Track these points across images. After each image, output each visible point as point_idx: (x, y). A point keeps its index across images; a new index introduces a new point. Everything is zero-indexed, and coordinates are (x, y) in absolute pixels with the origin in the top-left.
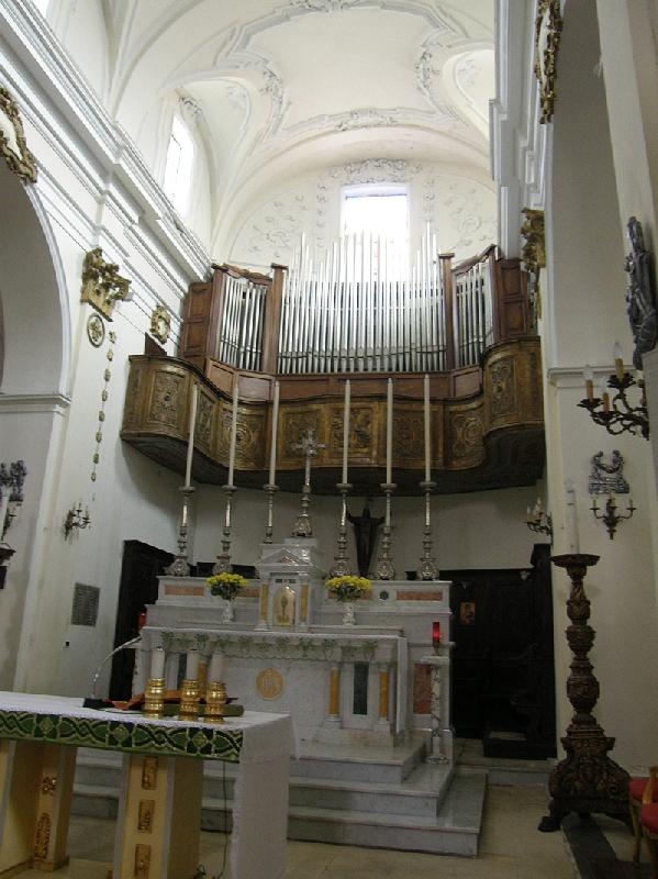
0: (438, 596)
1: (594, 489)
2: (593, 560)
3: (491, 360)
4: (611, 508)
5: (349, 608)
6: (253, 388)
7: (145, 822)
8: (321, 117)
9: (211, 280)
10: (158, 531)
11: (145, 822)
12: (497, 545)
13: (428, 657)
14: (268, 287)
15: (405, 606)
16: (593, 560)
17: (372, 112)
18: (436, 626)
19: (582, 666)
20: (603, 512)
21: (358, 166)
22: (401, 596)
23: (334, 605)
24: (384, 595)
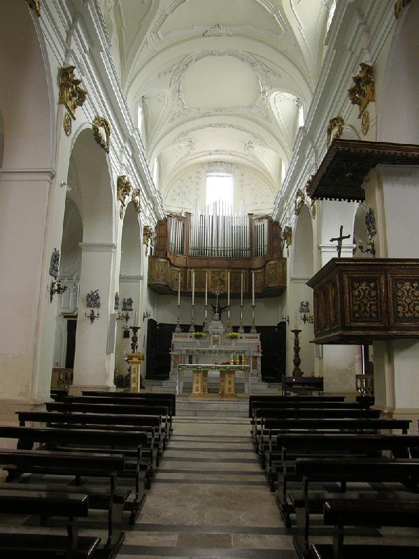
0: (257, 338)
1: (301, 312)
2: (300, 331)
3: (270, 263)
4: (305, 316)
5: (233, 341)
6: (180, 261)
7: (230, 383)
8: (205, 151)
9: (166, 220)
10: (164, 316)
11: (230, 383)
12: (269, 319)
13: (256, 354)
14: (185, 219)
15: (247, 341)
16: (300, 331)
17: (223, 151)
18: (258, 346)
19: (297, 355)
20: (303, 317)
21: (213, 165)
22: (246, 338)
23: (228, 341)
24: (241, 338)
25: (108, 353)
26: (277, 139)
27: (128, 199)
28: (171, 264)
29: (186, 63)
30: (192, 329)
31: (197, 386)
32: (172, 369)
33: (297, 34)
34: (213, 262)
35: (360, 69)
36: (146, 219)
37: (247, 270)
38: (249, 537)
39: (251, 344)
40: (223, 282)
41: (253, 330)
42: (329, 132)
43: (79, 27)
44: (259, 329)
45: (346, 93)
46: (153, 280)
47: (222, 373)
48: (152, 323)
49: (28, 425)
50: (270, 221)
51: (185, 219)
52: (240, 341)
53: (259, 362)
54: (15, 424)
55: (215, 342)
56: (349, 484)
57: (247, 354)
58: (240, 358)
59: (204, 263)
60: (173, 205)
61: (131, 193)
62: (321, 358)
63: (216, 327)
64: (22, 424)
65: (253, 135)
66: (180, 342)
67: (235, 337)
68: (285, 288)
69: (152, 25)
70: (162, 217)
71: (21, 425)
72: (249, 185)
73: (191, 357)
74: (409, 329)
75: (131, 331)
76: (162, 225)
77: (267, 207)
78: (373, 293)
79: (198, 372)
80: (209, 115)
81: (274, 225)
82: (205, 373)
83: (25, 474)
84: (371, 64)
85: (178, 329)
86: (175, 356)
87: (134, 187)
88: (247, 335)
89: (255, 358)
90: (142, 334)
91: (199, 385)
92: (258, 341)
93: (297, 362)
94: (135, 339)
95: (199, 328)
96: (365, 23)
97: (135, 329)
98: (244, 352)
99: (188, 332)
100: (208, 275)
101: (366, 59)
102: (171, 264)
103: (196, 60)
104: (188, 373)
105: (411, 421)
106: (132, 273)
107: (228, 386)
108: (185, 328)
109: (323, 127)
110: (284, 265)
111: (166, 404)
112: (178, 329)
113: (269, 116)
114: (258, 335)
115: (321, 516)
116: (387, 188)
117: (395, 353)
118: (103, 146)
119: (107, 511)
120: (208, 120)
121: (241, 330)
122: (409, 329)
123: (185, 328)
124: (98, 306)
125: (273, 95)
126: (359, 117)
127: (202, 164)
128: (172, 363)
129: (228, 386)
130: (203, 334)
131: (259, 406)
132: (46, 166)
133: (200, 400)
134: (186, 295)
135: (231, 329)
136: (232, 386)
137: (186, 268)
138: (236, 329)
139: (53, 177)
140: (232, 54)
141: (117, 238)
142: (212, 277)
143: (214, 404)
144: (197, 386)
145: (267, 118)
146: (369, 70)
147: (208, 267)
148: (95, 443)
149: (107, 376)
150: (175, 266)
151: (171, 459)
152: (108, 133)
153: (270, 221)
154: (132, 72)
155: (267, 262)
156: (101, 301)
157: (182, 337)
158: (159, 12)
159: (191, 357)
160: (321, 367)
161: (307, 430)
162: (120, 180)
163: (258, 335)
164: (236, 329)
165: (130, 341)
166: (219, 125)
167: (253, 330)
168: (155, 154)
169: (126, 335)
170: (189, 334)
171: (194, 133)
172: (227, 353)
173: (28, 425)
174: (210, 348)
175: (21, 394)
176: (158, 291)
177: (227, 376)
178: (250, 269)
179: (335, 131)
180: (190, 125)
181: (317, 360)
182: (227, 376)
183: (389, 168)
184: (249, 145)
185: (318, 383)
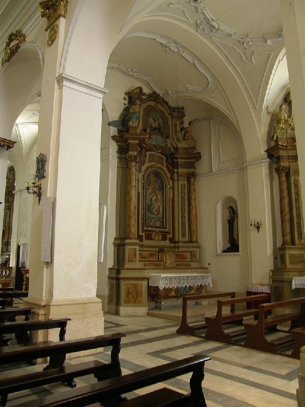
105: (70, 319)
126: (46, 30)
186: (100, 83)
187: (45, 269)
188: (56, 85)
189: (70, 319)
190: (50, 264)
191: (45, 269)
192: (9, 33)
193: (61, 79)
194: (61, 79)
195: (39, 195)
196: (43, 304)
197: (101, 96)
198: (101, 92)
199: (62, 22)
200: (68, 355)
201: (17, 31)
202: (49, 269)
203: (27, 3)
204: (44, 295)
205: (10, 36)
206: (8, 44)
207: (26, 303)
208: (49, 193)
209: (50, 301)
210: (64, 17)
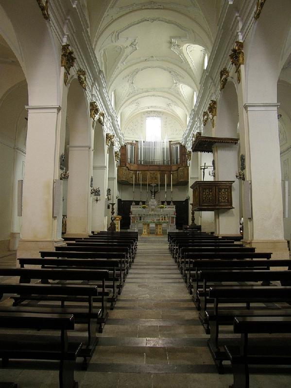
0: (173, 208)
6: (134, 167)
10: (126, 197)
12: (179, 197)
13: (173, 216)
22: (168, 208)
25: (105, 216)
26: (182, 102)
27: (97, 117)
28: (128, 169)
29: (137, 72)
30: (141, 203)
31: (145, 231)
32: (131, 224)
33: (191, 66)
34: (151, 167)
35: (236, 44)
36: (117, 148)
37: (170, 171)
38: (169, 297)
39: (171, 210)
40: (156, 178)
41: (172, 203)
42: (204, 117)
43: (96, 85)
44: (175, 203)
45: (229, 57)
46: (120, 178)
47: (156, 225)
48: (119, 201)
49: (27, 267)
50: (181, 146)
51: (135, 145)
52: (165, 209)
53: (175, 220)
54: (39, 257)
55: (153, 210)
56: (252, 305)
57: (169, 215)
58: (165, 217)
59: (146, 168)
60: (129, 137)
61: (98, 114)
62: (201, 217)
63: (153, 202)
64: (22, 266)
65: (172, 101)
66: (134, 209)
67: (163, 207)
68: (188, 182)
69: (121, 60)
70: (123, 144)
71: (21, 267)
72: (170, 124)
73: (140, 217)
74: (223, 206)
75: (111, 205)
76: (123, 148)
77: (179, 138)
78: (211, 193)
79: (145, 224)
80: (147, 91)
81: (183, 148)
82: (148, 225)
83: (33, 295)
84: (215, 100)
85: (134, 203)
86: (133, 217)
87: (101, 111)
88: (169, 206)
89: (173, 217)
90: (116, 206)
91: (146, 230)
92: (174, 209)
93: (193, 219)
94: (113, 209)
95: (144, 203)
96: (214, 82)
97: (113, 204)
98: (167, 215)
99: (139, 205)
100: (149, 174)
101: (214, 98)
102: (128, 169)
103: (142, 70)
104: (141, 225)
105: (272, 253)
106: (98, 164)
107: (159, 231)
108: (137, 203)
109: (217, 72)
110: (188, 170)
111: (134, 237)
112: (134, 203)
113: (179, 93)
114: (174, 206)
115: (231, 328)
116: (219, 152)
117: (220, 215)
118: (101, 124)
119: (102, 289)
120: (147, 94)
121: (166, 203)
122: (223, 206)
123: (137, 203)
124: (99, 195)
125: (181, 85)
126: (236, 72)
127: (144, 113)
128: (131, 221)
129: (159, 231)
130: (146, 206)
131: (172, 237)
132: (86, 144)
133: (147, 236)
134: (137, 185)
135: (161, 203)
136: (161, 230)
137: (137, 171)
138: (163, 203)
139: (90, 148)
140: (159, 67)
141: (107, 164)
142: (150, 176)
143: (153, 237)
144: (145, 231)
145: (178, 94)
146: (214, 103)
147: (148, 171)
148: (93, 263)
149: (104, 227)
150: (131, 170)
151: (129, 278)
152: (104, 118)
153: (181, 146)
154: (118, 109)
155: (179, 168)
156: (101, 193)
157: (137, 207)
158: (125, 55)
159: (140, 217)
160: (201, 220)
161: (221, 271)
162: (107, 135)
163: (174, 206)
164: (163, 203)
165: (111, 210)
166: (153, 95)
167: (172, 203)
168: (120, 111)
169: (109, 207)
170: (139, 206)
171: (139, 99)
172: (159, 215)
173: (27, 267)
174: (150, 213)
175: (83, 232)
176: (123, 184)
177: (159, 226)
178: (170, 171)
179: (224, 77)
180: (136, 97)
181: (199, 217)
182: (159, 226)
183: (220, 144)
184: (169, 105)
185: (199, 228)
186: (275, 101)
187: (249, 222)
188: (244, 109)
189: (272, 253)
190: (251, 219)
191: (249, 222)
192: (220, 71)
193: (246, 107)
194: (246, 107)
195: (244, 179)
196: (248, 242)
197: (276, 108)
198: (275, 106)
199: (242, 67)
200: (4, 294)
201: (224, 69)
202: (251, 222)
203: (245, 2)
204: (249, 237)
205: (221, 73)
206: (221, 78)
207: (243, 242)
208: (247, 178)
209: (252, 240)
210: (243, 64)
